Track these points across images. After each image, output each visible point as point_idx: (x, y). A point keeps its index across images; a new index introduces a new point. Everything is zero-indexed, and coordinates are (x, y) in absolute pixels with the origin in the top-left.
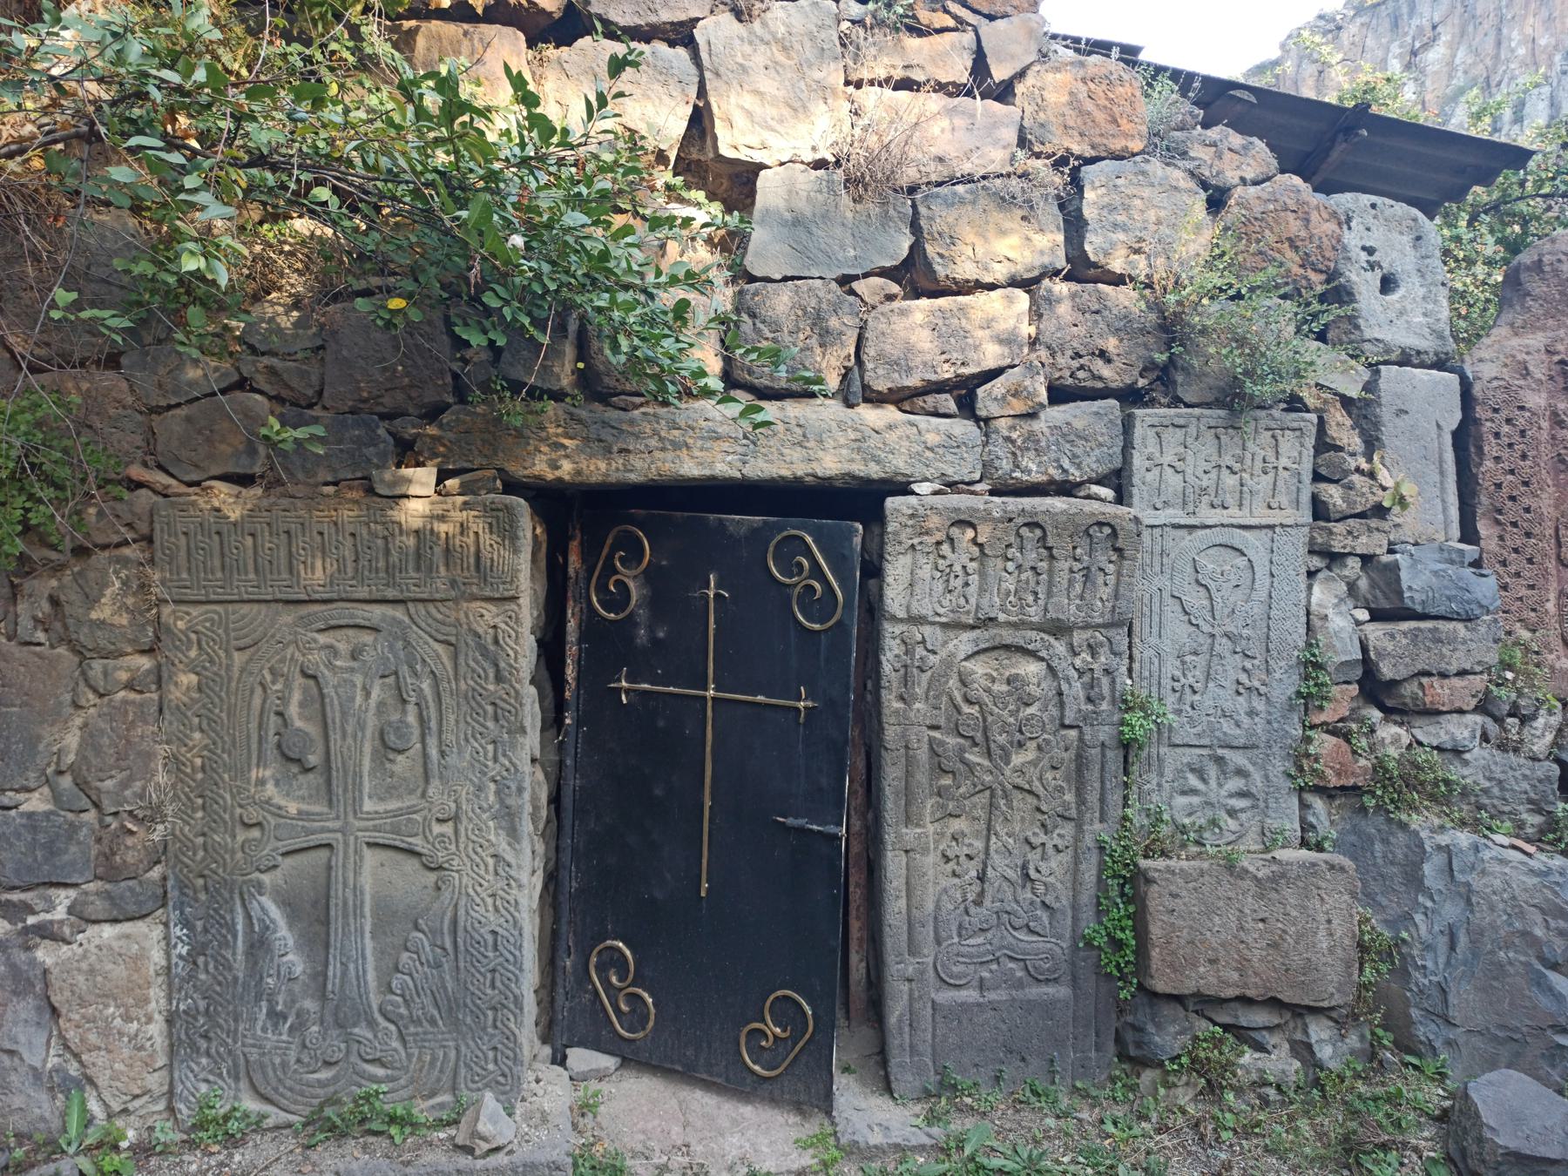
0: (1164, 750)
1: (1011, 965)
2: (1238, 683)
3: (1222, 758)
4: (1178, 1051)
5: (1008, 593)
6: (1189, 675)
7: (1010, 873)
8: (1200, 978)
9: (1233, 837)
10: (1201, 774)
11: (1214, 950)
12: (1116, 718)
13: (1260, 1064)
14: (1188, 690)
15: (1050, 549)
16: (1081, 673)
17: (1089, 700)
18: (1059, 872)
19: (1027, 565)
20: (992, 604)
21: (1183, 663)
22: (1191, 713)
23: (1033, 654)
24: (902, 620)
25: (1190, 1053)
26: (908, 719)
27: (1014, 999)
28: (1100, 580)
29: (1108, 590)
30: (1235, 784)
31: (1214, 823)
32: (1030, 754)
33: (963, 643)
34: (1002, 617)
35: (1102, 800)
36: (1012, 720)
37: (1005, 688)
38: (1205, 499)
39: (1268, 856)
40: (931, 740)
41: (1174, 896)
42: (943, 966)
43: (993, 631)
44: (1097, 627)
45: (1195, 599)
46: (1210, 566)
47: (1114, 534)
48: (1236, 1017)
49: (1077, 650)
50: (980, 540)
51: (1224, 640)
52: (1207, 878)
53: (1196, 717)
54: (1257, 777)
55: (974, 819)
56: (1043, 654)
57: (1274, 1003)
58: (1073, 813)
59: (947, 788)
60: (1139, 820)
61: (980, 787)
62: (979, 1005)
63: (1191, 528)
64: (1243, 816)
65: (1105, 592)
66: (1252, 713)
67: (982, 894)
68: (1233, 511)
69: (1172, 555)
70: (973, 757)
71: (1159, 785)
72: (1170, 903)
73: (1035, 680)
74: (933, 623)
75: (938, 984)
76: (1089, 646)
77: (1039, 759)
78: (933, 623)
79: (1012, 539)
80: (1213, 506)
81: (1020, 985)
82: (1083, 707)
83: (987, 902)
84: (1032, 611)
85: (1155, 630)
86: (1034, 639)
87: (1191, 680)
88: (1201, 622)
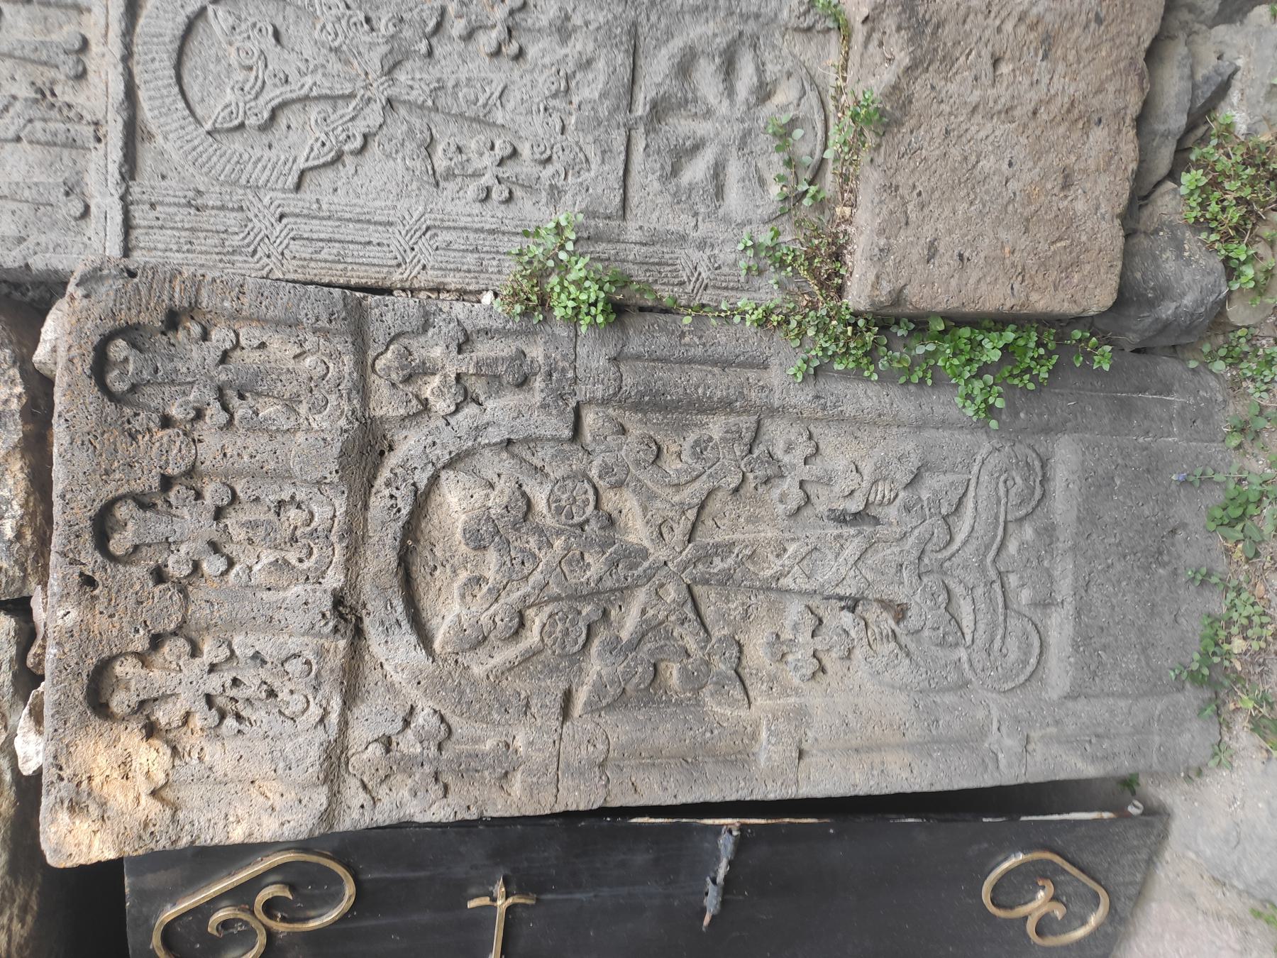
0: (632, 230)
1: (1012, 547)
2: (497, 53)
3: (654, 105)
4: (1216, 263)
5: (281, 565)
6: (477, 164)
7: (852, 550)
8: (1098, 201)
9: (812, 97)
10: (683, 153)
11: (1044, 177)
12: (562, 332)
13: (1257, 92)
14: (508, 171)
15: (167, 483)
16: (468, 397)
17: (523, 383)
18: (854, 451)
19: (210, 530)
20: (302, 600)
21: (450, 175)
22: (557, 166)
23: (422, 501)
24: (334, 795)
25: (1227, 239)
26: (542, 768)
27: (1074, 548)
28: (251, 358)
29: (275, 344)
30: (707, 79)
31: (784, 134)
32: (627, 504)
33: (393, 652)
34: (334, 579)
35: (725, 364)
36: (558, 543)
37: (492, 556)
38: (65, 93)
39: (859, 32)
40: (593, 708)
41: (932, 252)
42: (1006, 678)
43: (368, 590)
44: (363, 366)
45: (305, 138)
46: (229, 96)
47: (131, 333)
48: (1165, 135)
49: (415, 406)
50: (140, 642)
51: (402, 76)
52: (900, 179)
53: (567, 157)
54: (696, 31)
55: (746, 616)
56: (422, 479)
57: (1153, 54)
58: (746, 423)
59: (686, 675)
60: (769, 292)
61: (688, 610)
62: (1078, 613)
63: (133, 133)
64: (772, 70)
65: (281, 348)
66: (563, 30)
67: (885, 605)
68: (92, 26)
69: (201, 182)
70: (629, 622)
71: (702, 245)
72: (946, 259)
73: (479, 493)
74: (344, 724)
75: (1035, 683)
76: (408, 380)
77: (640, 490)
78: (344, 724)
79: (139, 571)
80: (81, 76)
81: (1048, 532)
82: (538, 398)
83: (899, 594)
84: (321, 513)
85: (375, 235)
86: (386, 506)
87: (488, 160)
88: (359, 128)
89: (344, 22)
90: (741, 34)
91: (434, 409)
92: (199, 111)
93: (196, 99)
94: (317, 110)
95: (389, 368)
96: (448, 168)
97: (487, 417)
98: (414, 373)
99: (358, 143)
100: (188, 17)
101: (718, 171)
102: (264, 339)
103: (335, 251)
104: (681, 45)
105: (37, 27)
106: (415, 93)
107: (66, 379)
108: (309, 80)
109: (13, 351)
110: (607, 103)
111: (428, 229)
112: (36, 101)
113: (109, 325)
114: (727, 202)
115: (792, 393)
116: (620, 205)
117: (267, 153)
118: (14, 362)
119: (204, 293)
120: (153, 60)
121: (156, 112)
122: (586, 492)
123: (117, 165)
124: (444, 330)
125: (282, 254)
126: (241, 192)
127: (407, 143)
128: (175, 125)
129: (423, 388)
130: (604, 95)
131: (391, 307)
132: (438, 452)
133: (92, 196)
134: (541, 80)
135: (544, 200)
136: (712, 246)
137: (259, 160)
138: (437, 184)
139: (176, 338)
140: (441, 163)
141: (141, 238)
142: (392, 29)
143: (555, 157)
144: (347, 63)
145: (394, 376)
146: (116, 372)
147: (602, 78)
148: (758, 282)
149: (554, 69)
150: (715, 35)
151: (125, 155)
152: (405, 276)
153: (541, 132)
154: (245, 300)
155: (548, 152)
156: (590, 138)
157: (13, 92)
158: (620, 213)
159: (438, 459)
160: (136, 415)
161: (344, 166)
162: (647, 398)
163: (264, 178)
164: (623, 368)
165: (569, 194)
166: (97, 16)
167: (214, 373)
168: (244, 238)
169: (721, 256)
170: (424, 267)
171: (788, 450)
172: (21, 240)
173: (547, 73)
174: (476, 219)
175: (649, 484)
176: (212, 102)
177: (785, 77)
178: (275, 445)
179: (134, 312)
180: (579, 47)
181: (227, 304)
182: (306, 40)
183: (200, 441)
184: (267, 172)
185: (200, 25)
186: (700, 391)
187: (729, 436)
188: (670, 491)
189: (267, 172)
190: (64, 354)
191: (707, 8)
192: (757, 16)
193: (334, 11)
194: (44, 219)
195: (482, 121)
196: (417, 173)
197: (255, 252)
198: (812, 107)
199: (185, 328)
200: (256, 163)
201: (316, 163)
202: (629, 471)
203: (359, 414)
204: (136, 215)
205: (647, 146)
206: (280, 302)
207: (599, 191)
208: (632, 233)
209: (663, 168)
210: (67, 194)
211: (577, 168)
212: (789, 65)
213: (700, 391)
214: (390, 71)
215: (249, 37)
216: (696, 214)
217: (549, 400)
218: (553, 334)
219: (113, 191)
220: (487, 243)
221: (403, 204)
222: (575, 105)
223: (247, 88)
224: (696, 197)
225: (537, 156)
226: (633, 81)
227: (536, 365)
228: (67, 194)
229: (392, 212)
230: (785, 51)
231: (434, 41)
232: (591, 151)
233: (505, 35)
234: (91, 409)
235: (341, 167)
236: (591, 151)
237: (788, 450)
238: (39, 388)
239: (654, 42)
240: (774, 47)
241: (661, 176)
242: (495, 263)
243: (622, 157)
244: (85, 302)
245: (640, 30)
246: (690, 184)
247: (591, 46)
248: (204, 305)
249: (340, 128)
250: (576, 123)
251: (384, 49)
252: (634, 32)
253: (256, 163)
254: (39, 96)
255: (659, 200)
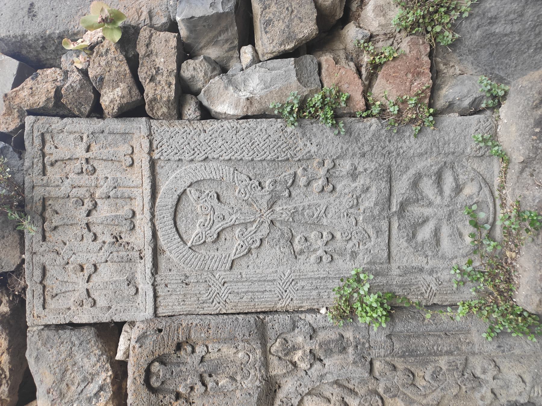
6: (315, 246)
9: (486, 190)
10: (416, 226)
14: (329, 249)
17: (343, 350)
21: (302, 252)
28: (214, 355)
30: (428, 187)
44: (266, 352)
45: (233, 245)
51: (277, 208)
58: (460, 362)
63: (156, 252)
65: (227, 351)
69: (187, 270)
71: (431, 272)
82: (351, 359)
87: (320, 243)
88: (259, 236)
89: (249, 187)
90: (445, 163)
91: (299, 366)
92: (185, 237)
93: (183, 231)
94: (239, 230)
95: (277, 351)
96: (301, 250)
97: (326, 370)
98: (289, 350)
99: (258, 244)
100: (178, 195)
101: (436, 233)
102: (220, 348)
103: (249, 297)
104: (414, 172)
105: (113, 208)
106: (283, 216)
107: (133, 388)
108: (234, 217)
109: (107, 356)
110: (378, 208)
111: (293, 280)
112: (113, 243)
113: (151, 358)
114: (442, 247)
115: (485, 346)
116: (387, 257)
117: (216, 253)
118: (108, 361)
119: (192, 332)
120: (164, 217)
121: (166, 241)
122: (377, 402)
123: (150, 269)
124: (303, 329)
125: (225, 301)
126: (205, 274)
127: (281, 240)
128: (174, 246)
129: (294, 357)
130: (376, 204)
131: (277, 321)
132: (303, 389)
133: (139, 284)
134: (344, 201)
135: (348, 259)
136: (437, 272)
137: (213, 258)
138: (296, 257)
139: (180, 354)
140: (297, 247)
141: (162, 301)
142: (272, 187)
143: (353, 237)
144: (251, 205)
145: (280, 354)
146: (155, 378)
147: (374, 196)
148: (462, 288)
149: (350, 195)
150: (431, 166)
151: (153, 264)
152: (283, 305)
153: (345, 226)
154: (211, 332)
155: (350, 236)
156: (370, 226)
157: (103, 239)
158: (388, 261)
159: (303, 392)
160: (165, 397)
161: (252, 254)
162: (407, 354)
163: (216, 266)
164: (393, 340)
165: (361, 254)
166: (139, 200)
167: (198, 368)
168: (208, 296)
169: (442, 277)
170: (292, 299)
171: (484, 372)
172: (110, 308)
173: (347, 197)
174: (316, 273)
175: (410, 395)
176: (190, 232)
177: (470, 181)
178: (227, 399)
179: (162, 349)
180: (362, 182)
181: (203, 335)
182: (232, 197)
183: (193, 403)
184: (217, 263)
185: (184, 197)
186: (435, 348)
187: (451, 368)
188: (421, 398)
189: (217, 263)
190: (132, 376)
191: (426, 153)
192: (453, 153)
193: (244, 183)
194: (119, 297)
195: (317, 224)
196: (286, 254)
197: (213, 301)
198: (486, 195)
199: (184, 349)
200: (212, 259)
201: (239, 256)
202: (399, 389)
203: (265, 376)
204: (159, 290)
205: (399, 225)
206: (226, 330)
207: (376, 251)
208: (395, 272)
209: (408, 235)
210: (128, 285)
211: (364, 241)
212: (472, 174)
213: (435, 348)
214: (271, 206)
215: (206, 201)
216: (427, 256)
217: (357, 359)
218: (357, 326)
219: (148, 282)
220: (322, 284)
221: (281, 269)
222: (362, 211)
223: (206, 225)
224: (426, 248)
225: (344, 239)
226: (390, 194)
227: (349, 342)
228: (128, 285)
229: (275, 274)
230: (469, 168)
231: (291, 189)
232: (371, 232)
233: (326, 182)
234: (145, 400)
235: (250, 255)
236: (371, 232)
237: (484, 372)
238: (120, 370)
239: (399, 173)
240: (463, 167)
241: (407, 239)
242: (326, 294)
243: (387, 233)
244: (140, 349)
245: (392, 169)
246: (422, 242)
247: (368, 181)
248: (192, 337)
249: (250, 238)
250: (363, 220)
251: (268, 197)
252: (389, 172)
253: (212, 259)
254: (115, 240)
255: (407, 251)
